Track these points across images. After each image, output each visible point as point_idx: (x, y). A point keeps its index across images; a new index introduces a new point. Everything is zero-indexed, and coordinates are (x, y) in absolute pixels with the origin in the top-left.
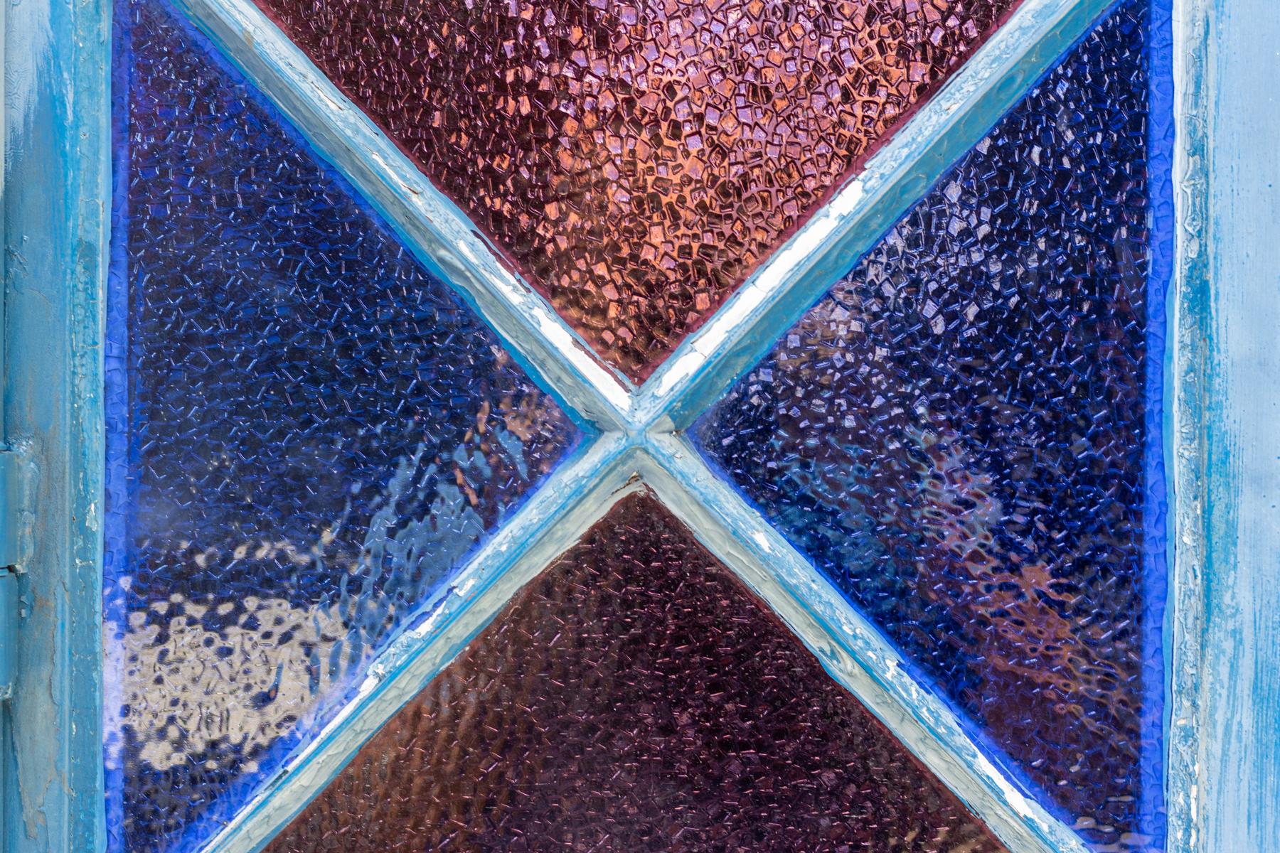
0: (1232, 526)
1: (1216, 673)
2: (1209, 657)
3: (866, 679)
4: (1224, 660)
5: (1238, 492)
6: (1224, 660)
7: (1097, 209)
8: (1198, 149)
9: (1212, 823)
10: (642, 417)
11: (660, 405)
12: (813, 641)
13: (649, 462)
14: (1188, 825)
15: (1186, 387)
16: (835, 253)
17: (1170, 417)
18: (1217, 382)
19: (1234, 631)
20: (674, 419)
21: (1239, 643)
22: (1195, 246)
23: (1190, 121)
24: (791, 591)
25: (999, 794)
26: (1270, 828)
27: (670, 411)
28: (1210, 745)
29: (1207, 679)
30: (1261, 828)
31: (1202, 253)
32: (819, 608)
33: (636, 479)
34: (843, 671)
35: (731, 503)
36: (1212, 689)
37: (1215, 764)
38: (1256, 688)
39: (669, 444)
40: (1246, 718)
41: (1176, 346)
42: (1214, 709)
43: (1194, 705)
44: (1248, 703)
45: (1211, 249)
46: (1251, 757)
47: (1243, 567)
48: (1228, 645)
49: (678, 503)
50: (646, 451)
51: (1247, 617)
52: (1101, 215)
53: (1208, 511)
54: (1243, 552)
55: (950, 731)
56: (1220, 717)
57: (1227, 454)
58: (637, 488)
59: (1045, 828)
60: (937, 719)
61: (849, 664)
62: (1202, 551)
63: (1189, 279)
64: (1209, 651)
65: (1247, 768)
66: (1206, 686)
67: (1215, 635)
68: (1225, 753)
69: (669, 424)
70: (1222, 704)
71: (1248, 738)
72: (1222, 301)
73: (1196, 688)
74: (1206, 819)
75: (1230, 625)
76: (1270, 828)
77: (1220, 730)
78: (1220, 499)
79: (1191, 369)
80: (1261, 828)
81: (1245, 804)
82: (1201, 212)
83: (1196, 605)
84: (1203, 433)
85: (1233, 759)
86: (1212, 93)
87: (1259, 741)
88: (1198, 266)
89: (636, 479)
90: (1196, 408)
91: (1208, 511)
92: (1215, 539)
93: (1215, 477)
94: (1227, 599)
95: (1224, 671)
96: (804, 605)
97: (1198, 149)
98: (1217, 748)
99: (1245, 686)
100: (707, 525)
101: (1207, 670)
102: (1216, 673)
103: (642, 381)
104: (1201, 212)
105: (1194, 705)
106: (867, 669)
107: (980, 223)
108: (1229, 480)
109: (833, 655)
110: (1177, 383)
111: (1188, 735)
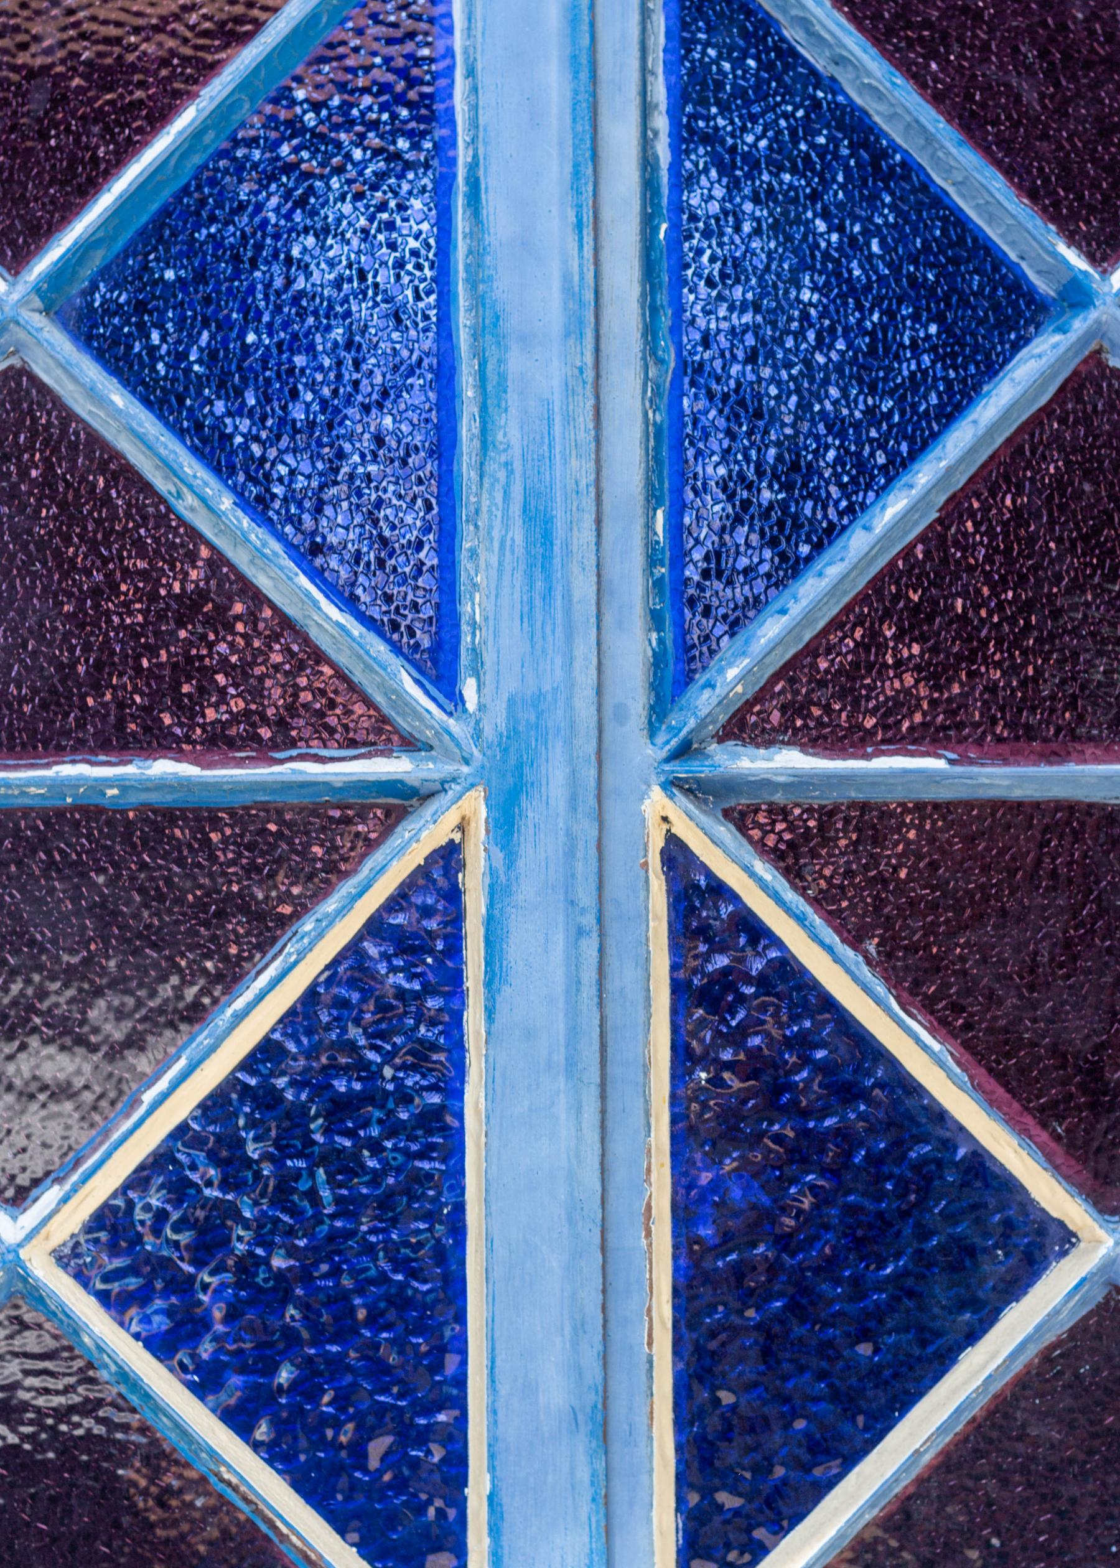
0: (502, 377)
1: (492, 497)
2: (486, 485)
3: (203, 511)
4: (499, 487)
5: (507, 349)
6: (499, 487)
7: (1009, 650)
8: (471, 73)
9: (491, 623)
10: (15, 296)
11: (29, 287)
12: (162, 485)
13: (22, 335)
14: (473, 624)
15: (467, 267)
16: (173, 162)
17: (456, 295)
18: (488, 259)
19: (506, 464)
20: (42, 299)
21: (510, 473)
22: (470, 152)
23: (466, 51)
24: (140, 438)
25: (315, 603)
26: (539, 624)
27: (37, 290)
28: (489, 557)
29: (485, 504)
30: (531, 626)
31: (475, 156)
32: (162, 451)
33: (13, 353)
34: (187, 506)
35: (91, 370)
36: (489, 511)
37: (493, 573)
38: (525, 509)
39: (38, 320)
40: (517, 534)
41: (460, 236)
42: (491, 527)
43: (476, 527)
44: (519, 522)
45: (481, 152)
46: (522, 567)
47: (513, 411)
48: (502, 475)
49: (47, 371)
50: (18, 323)
51: (517, 451)
52: (1012, 656)
53: (483, 365)
54: (512, 398)
55: (275, 554)
56: (496, 534)
57: (498, 318)
58: (15, 361)
59: (356, 633)
60: (264, 545)
61: (190, 499)
62: (479, 399)
63: (467, 180)
64: (486, 480)
65: (519, 577)
66: (484, 509)
67: (491, 467)
68: (500, 564)
69: (38, 303)
70: (497, 523)
71: (520, 551)
72: (491, 193)
73: (477, 512)
74: (486, 619)
75: (503, 458)
76: (539, 624)
77: (496, 545)
78: (492, 353)
79: (470, 252)
80: (531, 626)
81: (518, 606)
82: (474, 124)
83: (476, 443)
84: (479, 302)
85: (508, 568)
86: (480, 25)
87: (528, 553)
88: (473, 166)
89: (13, 353)
90: (473, 283)
91: (483, 365)
92: (489, 388)
93: (488, 337)
94: (500, 437)
95: (499, 496)
96: (149, 447)
97: (471, 73)
98: (494, 560)
99: (516, 509)
100: (71, 386)
101: (485, 496)
102: (492, 497)
103: (17, 273)
104: (474, 124)
105: (476, 527)
106: (203, 500)
107: (761, 561)
108: (500, 341)
109: (179, 496)
110: (461, 267)
111: (473, 554)
